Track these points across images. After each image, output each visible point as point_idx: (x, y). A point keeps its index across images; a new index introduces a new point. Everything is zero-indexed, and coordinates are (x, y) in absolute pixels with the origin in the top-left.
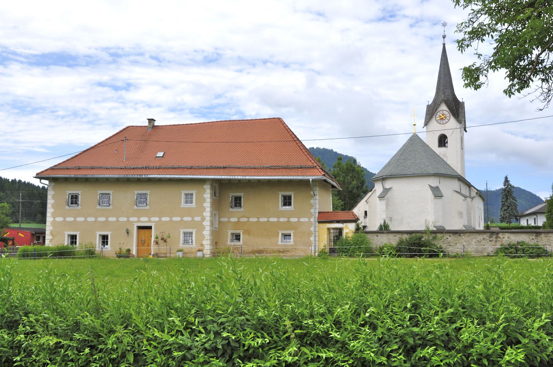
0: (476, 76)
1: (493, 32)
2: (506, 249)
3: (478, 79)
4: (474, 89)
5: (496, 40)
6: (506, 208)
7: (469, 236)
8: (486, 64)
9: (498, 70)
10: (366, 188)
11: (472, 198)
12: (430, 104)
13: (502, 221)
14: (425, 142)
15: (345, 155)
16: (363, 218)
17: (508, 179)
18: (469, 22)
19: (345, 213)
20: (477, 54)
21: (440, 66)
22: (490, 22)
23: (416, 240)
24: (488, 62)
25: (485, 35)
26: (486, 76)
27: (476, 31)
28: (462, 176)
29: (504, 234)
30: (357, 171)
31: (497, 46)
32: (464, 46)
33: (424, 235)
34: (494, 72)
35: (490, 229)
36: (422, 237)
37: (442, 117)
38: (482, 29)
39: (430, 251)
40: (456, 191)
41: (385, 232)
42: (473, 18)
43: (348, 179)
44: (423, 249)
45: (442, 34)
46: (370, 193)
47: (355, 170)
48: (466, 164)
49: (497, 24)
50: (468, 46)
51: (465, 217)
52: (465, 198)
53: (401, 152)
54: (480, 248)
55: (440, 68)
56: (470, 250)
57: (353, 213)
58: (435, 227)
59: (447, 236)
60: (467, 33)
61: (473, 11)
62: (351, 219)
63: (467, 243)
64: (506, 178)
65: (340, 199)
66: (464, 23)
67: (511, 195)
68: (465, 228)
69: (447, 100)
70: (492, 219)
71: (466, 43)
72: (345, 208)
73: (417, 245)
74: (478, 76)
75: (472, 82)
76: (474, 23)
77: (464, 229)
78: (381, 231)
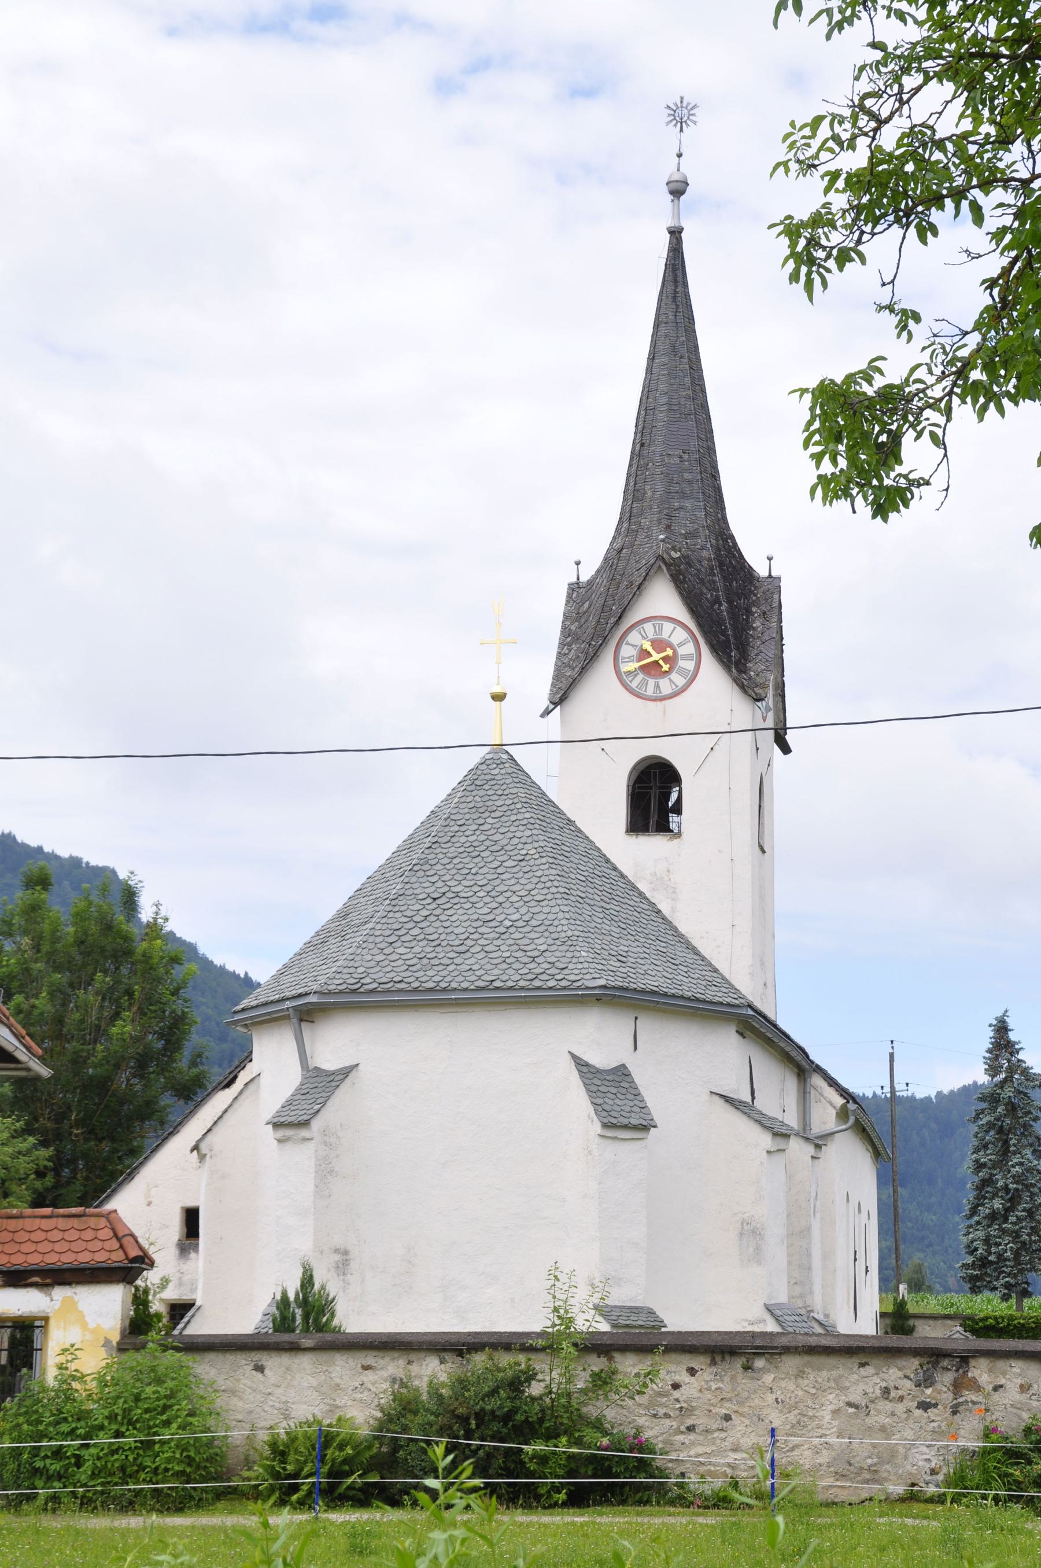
0: (883, 438)
1: (986, 186)
2: (1014, 1455)
3: (890, 453)
4: (869, 511)
5: (998, 235)
6: (997, 1204)
7: (801, 1374)
8: (938, 371)
9: (1001, 411)
10: (194, 1064)
11: (818, 1143)
12: (585, 578)
13: (976, 1285)
14: (552, 795)
15: (64, 853)
16: (173, 1251)
17: (1013, 1036)
18: (855, 118)
19: (61, 1223)
20: (890, 308)
21: (652, 358)
22: (967, 125)
23: (494, 1392)
24: (952, 363)
25: (937, 201)
26: (938, 441)
27: (889, 173)
28: (758, 1004)
29: (1001, 1364)
30: (146, 957)
31: (1006, 271)
32: (821, 254)
33: (540, 1363)
34: (981, 419)
35: (909, 1331)
36: (530, 1376)
37: (656, 656)
38: (922, 163)
39: (573, 1466)
40: (727, 1099)
41: (307, 1342)
42: (876, 95)
43: (86, 1008)
44: (535, 1456)
45: (668, 170)
46: (221, 1099)
47: (129, 953)
48: (782, 936)
49: (1005, 141)
50: (843, 257)
51: (777, 1253)
52: (781, 1143)
53: (416, 856)
54: (863, 1448)
55: (649, 370)
56: (805, 1458)
57: (112, 1218)
58: (602, 1310)
59: (674, 1369)
60: (840, 184)
61: (878, 55)
62: (101, 1257)
63: (792, 1417)
64: (1002, 1028)
65: (28, 1131)
66: (826, 123)
67: (1026, 1126)
68: (777, 1319)
69: (686, 560)
70: (919, 1269)
71: (836, 238)
72: (57, 1185)
73: (495, 1426)
74: (896, 438)
75: (861, 472)
76: (881, 122)
77: (771, 1326)
78: (286, 1337)
